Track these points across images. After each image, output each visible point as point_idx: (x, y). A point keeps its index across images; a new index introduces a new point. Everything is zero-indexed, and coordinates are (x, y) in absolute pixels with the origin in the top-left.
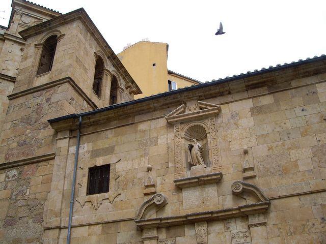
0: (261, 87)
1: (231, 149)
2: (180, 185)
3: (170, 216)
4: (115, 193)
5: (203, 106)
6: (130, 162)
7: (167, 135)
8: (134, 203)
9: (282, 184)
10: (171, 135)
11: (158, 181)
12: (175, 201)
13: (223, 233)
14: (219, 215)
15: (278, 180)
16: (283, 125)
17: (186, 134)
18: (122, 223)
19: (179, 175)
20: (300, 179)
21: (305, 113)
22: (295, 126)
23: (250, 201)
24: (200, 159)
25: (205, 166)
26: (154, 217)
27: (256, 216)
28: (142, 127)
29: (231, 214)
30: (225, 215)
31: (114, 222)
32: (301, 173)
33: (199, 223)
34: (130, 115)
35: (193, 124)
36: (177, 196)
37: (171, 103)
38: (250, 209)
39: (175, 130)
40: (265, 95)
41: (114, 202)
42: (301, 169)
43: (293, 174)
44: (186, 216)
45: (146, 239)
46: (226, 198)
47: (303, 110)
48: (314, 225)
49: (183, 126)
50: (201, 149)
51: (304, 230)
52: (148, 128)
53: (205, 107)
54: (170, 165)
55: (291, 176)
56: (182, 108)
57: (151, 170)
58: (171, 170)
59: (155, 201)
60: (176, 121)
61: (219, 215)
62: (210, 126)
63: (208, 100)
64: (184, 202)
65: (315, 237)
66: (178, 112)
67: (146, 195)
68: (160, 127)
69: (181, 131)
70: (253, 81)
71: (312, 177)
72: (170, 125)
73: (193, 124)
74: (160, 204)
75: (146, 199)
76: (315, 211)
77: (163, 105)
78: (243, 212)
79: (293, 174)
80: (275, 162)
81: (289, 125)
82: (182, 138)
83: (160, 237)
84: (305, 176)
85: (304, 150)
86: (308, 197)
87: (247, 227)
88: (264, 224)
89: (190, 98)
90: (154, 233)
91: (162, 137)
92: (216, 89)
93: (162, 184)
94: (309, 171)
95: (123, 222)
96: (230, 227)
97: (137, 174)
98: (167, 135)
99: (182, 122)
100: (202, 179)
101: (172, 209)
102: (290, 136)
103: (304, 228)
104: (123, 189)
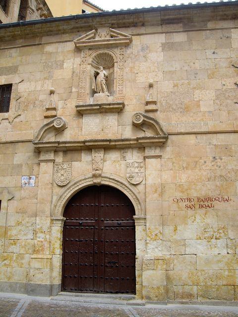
2: (81, 110)
3: (68, 140)
5: (114, 34)
7: (74, 59)
9: (182, 121)
10: (78, 60)
11: (60, 105)
12: (75, 126)
14: (117, 143)
16: (192, 64)
17: (94, 61)
21: (215, 56)
23: (149, 133)
26: (53, 140)
27: (153, 148)
28: (49, 48)
29: (129, 144)
31: (12, 142)
33: (96, 150)
34: (38, 34)
35: (101, 51)
36: (76, 122)
38: (148, 141)
39: (82, 56)
40: (179, 32)
41: (13, 123)
44: (84, 142)
47: (214, 53)
48: (205, 162)
49: (91, 52)
50: (107, 77)
52: (54, 51)
53: (116, 35)
54: (74, 90)
55: (192, 114)
56: (92, 33)
57: (53, 94)
58: (74, 95)
59: (55, 124)
60: (85, 46)
61: (117, 143)
63: (120, 29)
65: (205, 173)
66: (87, 38)
67: (46, 117)
70: (169, 15)
72: (78, 49)
73: (101, 51)
74: (59, 128)
75: (47, 121)
76: (208, 150)
78: (141, 143)
81: (197, 65)
86: (204, 136)
87: (143, 158)
88: (160, 157)
89: (101, 24)
90: (51, 156)
93: (63, 108)
95: (21, 143)
96: (127, 157)
98: (74, 59)
99: (91, 47)
102: (197, 76)
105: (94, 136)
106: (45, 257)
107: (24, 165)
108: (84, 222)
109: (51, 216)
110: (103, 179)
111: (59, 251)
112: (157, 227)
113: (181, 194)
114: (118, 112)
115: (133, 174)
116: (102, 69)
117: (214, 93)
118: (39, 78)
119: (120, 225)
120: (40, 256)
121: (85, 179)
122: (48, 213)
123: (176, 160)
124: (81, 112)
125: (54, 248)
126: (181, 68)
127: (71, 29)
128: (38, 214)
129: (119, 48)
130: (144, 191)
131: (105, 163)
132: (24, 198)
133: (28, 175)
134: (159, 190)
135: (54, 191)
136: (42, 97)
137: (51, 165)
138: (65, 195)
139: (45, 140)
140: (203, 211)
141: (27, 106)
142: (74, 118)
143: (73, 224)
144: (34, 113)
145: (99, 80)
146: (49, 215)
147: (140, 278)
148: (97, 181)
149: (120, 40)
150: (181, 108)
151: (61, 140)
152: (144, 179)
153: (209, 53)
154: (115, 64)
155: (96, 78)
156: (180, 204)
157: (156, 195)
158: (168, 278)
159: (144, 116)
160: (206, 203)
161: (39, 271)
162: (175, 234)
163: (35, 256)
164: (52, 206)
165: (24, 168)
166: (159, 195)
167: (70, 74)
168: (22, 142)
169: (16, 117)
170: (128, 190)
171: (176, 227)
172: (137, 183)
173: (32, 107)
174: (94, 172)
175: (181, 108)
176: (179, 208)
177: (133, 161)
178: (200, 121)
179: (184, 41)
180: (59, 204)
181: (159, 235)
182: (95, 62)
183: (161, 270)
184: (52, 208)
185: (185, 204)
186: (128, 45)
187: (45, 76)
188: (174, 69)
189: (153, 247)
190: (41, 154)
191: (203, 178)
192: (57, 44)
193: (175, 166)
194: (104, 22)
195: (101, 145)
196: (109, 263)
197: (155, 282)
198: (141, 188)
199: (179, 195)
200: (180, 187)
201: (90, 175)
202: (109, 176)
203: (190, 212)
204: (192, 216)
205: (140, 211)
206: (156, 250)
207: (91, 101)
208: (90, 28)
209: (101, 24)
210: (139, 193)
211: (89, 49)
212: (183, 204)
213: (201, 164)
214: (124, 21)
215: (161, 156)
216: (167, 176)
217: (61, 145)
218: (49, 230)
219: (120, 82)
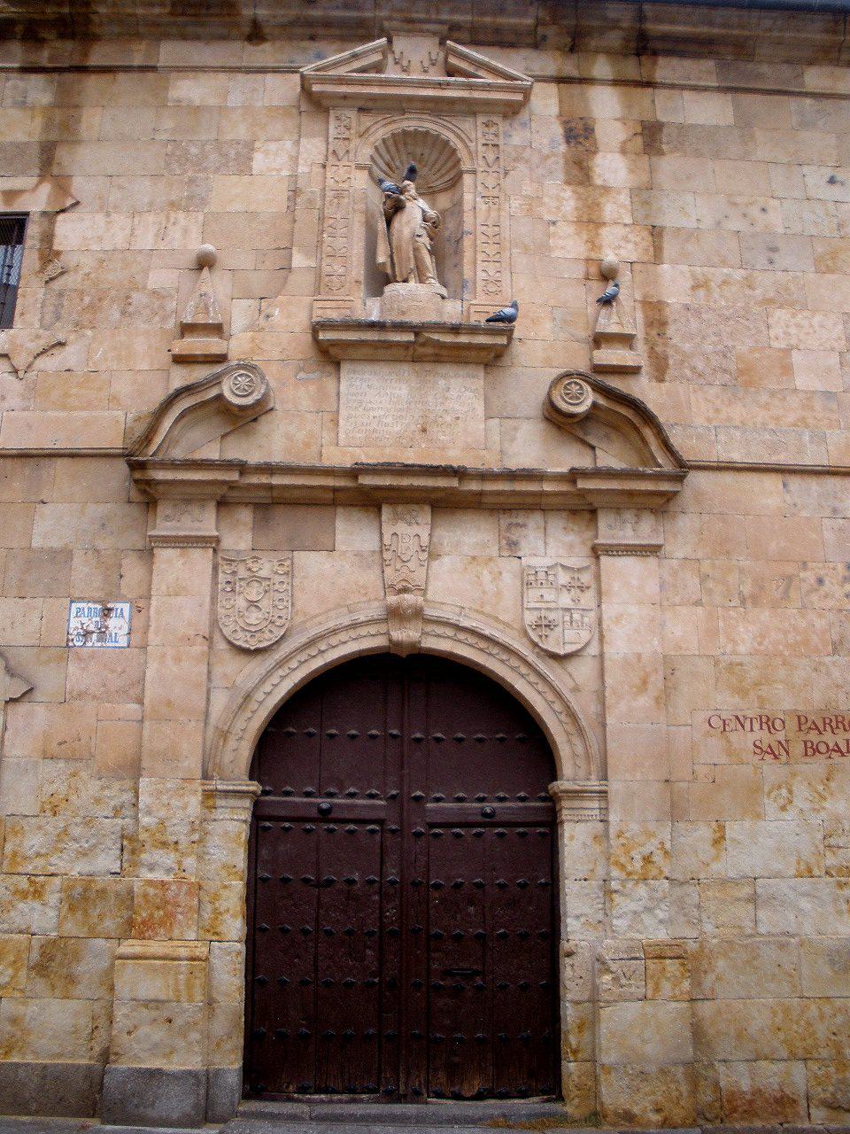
0: (697, 56)
1: (550, 249)
2: (334, 343)
3: (277, 457)
4: (38, 337)
5: (464, 65)
6: (120, 220)
7: (297, 143)
8: (122, 387)
9: (729, 419)
10: (313, 148)
11: (239, 316)
12: (305, 404)
13: (491, 559)
14: (490, 487)
15: (718, 402)
16: (754, 212)
17: (377, 157)
18: (60, 462)
19: (333, 304)
20: (791, 418)
21: (835, 192)
22: (797, 228)
23: (611, 456)
24: (428, 260)
25: (444, 292)
26: (212, 452)
27: (629, 516)
28: (189, 90)
29: (533, 494)
30: (514, 493)
31: (24, 456)
32: (801, 396)
33: (400, 508)
34: (142, 30)
35: (411, 123)
36: (312, 388)
37: (327, 24)
38: (614, 485)
39: (332, 131)
40: (706, 89)
41: (32, 375)
42: (801, 381)
43: (773, 394)
44: (355, 472)
45: (168, 541)
46: (515, 429)
47: (832, 181)
48: (820, 581)
49: (367, 121)
50: (435, 225)
51: (786, 595)
52: (212, 101)
53: (471, 69)
54: (298, 260)
55: (764, 398)
56: (374, 50)
57: (211, 267)
58: (301, 281)
59: (227, 389)
60: (345, 97)
61: (490, 487)
62: (481, 148)
63: (481, 48)
64: (343, 412)
65: (820, 624)
66: (357, 65)
67: (180, 360)
68: (270, 109)
69: (355, 142)
70: (672, 22)
71: (835, 416)
72: (316, 103)
73: (411, 123)
74: (242, 408)
75: (180, 377)
76: (829, 536)
77: (293, 23)
78: (583, 493)
79: (773, 394)
80: (714, 339)
81: (776, 219)
82: (360, 167)
83: (228, 542)
84: (812, 409)
85: (818, 319)
86: (814, 485)
87: (586, 550)
88: (652, 550)
89: (410, 21)
90: (205, 522)
91: (273, 146)
92: (524, 14)
93: (252, 327)
94: (828, 395)
95: (66, 461)
96: (523, 544)
97: (146, 272)
98: (297, 143)
99: (370, 104)
100: (435, 337)
101: (289, 438)
102: (775, 256)
103: (786, 591)
104: (78, 325)
105: (388, 451)
106: (183, 952)
107: (78, 560)
108: (339, 806)
109: (206, 776)
110: (429, 628)
111: (235, 927)
112: (652, 826)
113: (737, 699)
114: (486, 365)
115: (551, 616)
116: (413, 192)
117: (841, 327)
118: (146, 200)
119: (489, 820)
120: (155, 947)
121: (354, 626)
122: (193, 764)
123: (713, 566)
124: (333, 351)
125: (217, 913)
126: (719, 223)
127: (283, 26)
128: (144, 764)
129: (481, 119)
130: (593, 685)
131: (435, 564)
132: (80, 695)
133: (97, 595)
134: (656, 681)
135: (218, 670)
136: (161, 278)
137: (201, 559)
138: (267, 687)
139: (178, 453)
140: (818, 765)
141: (93, 308)
142: (302, 375)
143: (291, 814)
144: (123, 338)
145: (406, 232)
146: (199, 774)
147: (586, 1035)
148: (406, 634)
149: (486, 86)
150: (725, 371)
151: (254, 458)
152: (596, 636)
153: (815, 178)
154: (467, 179)
155: (389, 222)
156: (734, 737)
157: (644, 701)
158: (698, 1033)
159: (600, 389)
160: (829, 738)
161: (155, 1014)
162: (717, 858)
163: (131, 947)
164: (211, 731)
165: (82, 570)
166: (657, 700)
167: (282, 196)
168: (72, 456)
169: (44, 351)
170: (533, 678)
171: (722, 828)
172: (569, 649)
173: (116, 315)
174: (392, 599)
175: (725, 371)
176: (729, 754)
177: (548, 562)
178: (795, 425)
179: (722, 123)
180: (240, 724)
181: (658, 858)
182: (380, 162)
183: (675, 999)
184: (208, 743)
185: (751, 737)
186: (516, 113)
187: (173, 198)
188: (693, 225)
189: (633, 906)
190: (163, 509)
191: (815, 639)
192: (222, 77)
193: (710, 592)
194: (422, 16)
195: (419, 489)
196: (447, 973)
197: (651, 1049)
198: (583, 671)
199: (727, 702)
200: (730, 672)
201: (375, 610)
202: (454, 619)
203: (771, 771)
204: (779, 787)
205: (581, 762)
206: (647, 918)
207: (373, 310)
208: (361, 32)
209: (410, 21)
210: (576, 689)
211: (361, 110)
212: (745, 740)
213: (805, 587)
214: (502, 20)
215: (659, 547)
216: (683, 628)
217: (254, 480)
218: (196, 837)
219: (491, 250)
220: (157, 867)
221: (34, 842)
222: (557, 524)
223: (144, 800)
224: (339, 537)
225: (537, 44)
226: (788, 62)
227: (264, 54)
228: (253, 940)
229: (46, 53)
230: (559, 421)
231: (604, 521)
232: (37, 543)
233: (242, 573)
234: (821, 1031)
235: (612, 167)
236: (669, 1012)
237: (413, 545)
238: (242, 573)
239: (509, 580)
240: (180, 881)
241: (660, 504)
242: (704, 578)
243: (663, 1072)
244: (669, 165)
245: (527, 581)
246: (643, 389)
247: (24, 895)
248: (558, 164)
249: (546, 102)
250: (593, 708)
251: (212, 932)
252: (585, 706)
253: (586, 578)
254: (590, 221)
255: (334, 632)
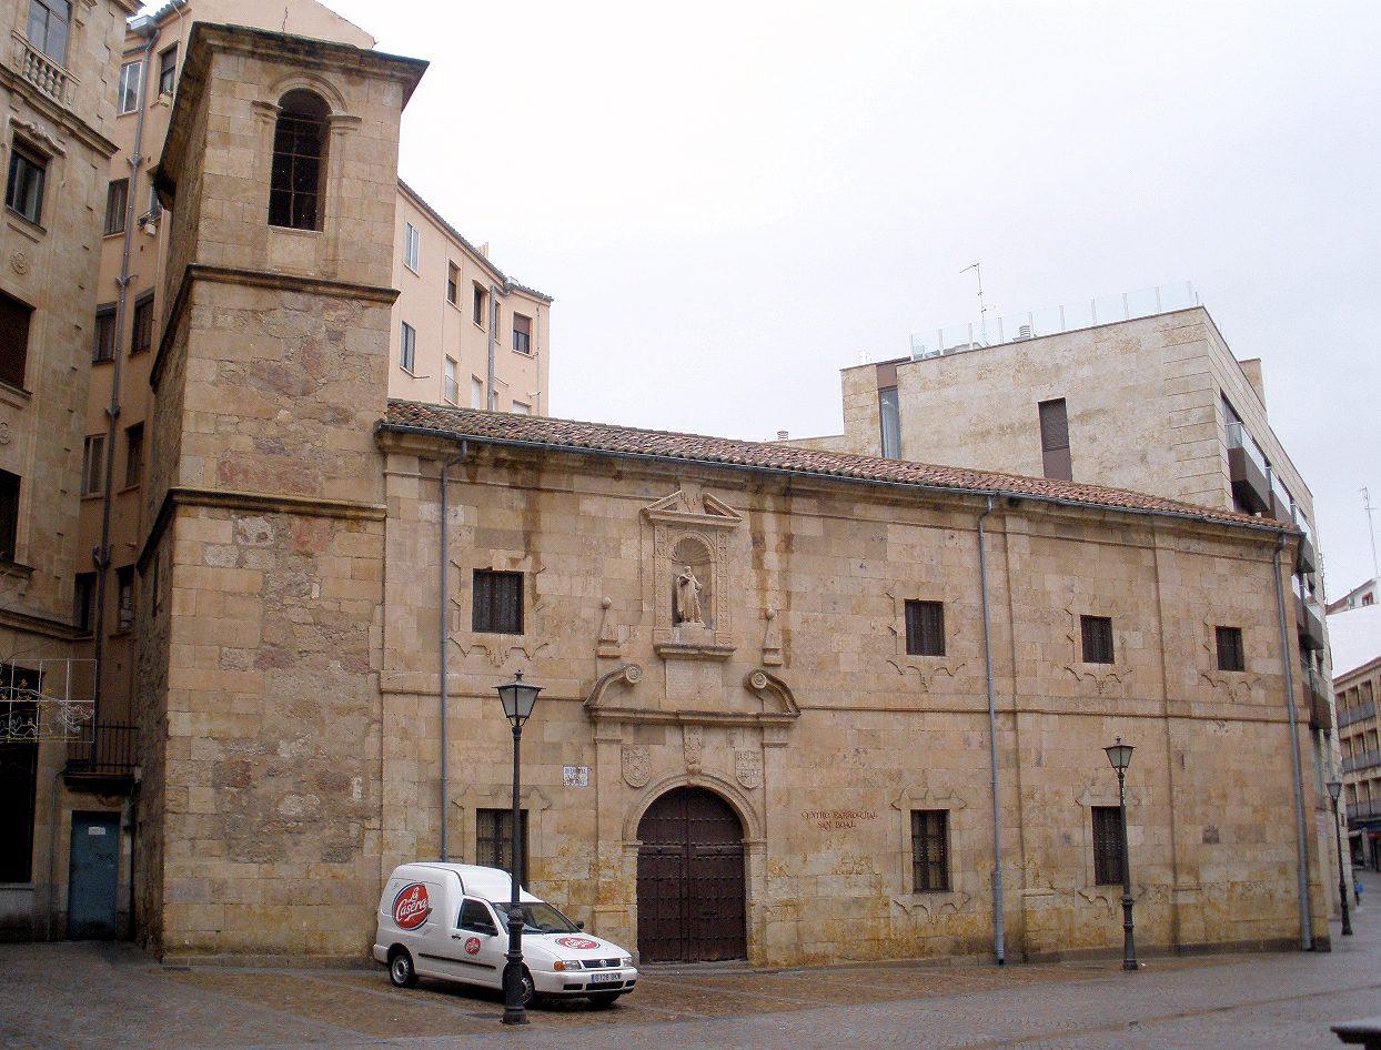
11: (621, 635)
23: (770, 706)
28: (589, 506)
35: (688, 535)
38: (773, 720)
44: (677, 714)
54: (646, 608)
73: (688, 535)
94: (853, 674)
113: (812, 806)
119: (719, 853)
121: (675, 777)
137: (616, 749)
140: (841, 832)
148: (696, 781)
157: (779, 806)
163: (599, 908)
165: (567, 752)
198: (758, 795)
199: (808, 807)
203: (824, 834)
210: (755, 802)
220: (606, 877)
221: (556, 867)
222: (748, 733)
223: (601, 849)
224: (668, 739)
225: (742, 488)
226: (847, 501)
227: (621, 487)
228: (640, 903)
229: (519, 477)
230: (750, 688)
231: (767, 733)
232: (546, 739)
233: (632, 754)
234: (855, 564)
235: (772, 559)
236: (789, 925)
237: (696, 742)
238: (632, 754)
239: (731, 757)
240: (616, 881)
241: (786, 727)
242: (802, 756)
243: (787, 947)
244: (795, 557)
245: (737, 757)
246: (781, 674)
247: (554, 889)
248: (749, 557)
249: (745, 517)
250: (761, 809)
251: (627, 901)
252: (759, 809)
253: (760, 756)
254: (762, 589)
255: (668, 779)
